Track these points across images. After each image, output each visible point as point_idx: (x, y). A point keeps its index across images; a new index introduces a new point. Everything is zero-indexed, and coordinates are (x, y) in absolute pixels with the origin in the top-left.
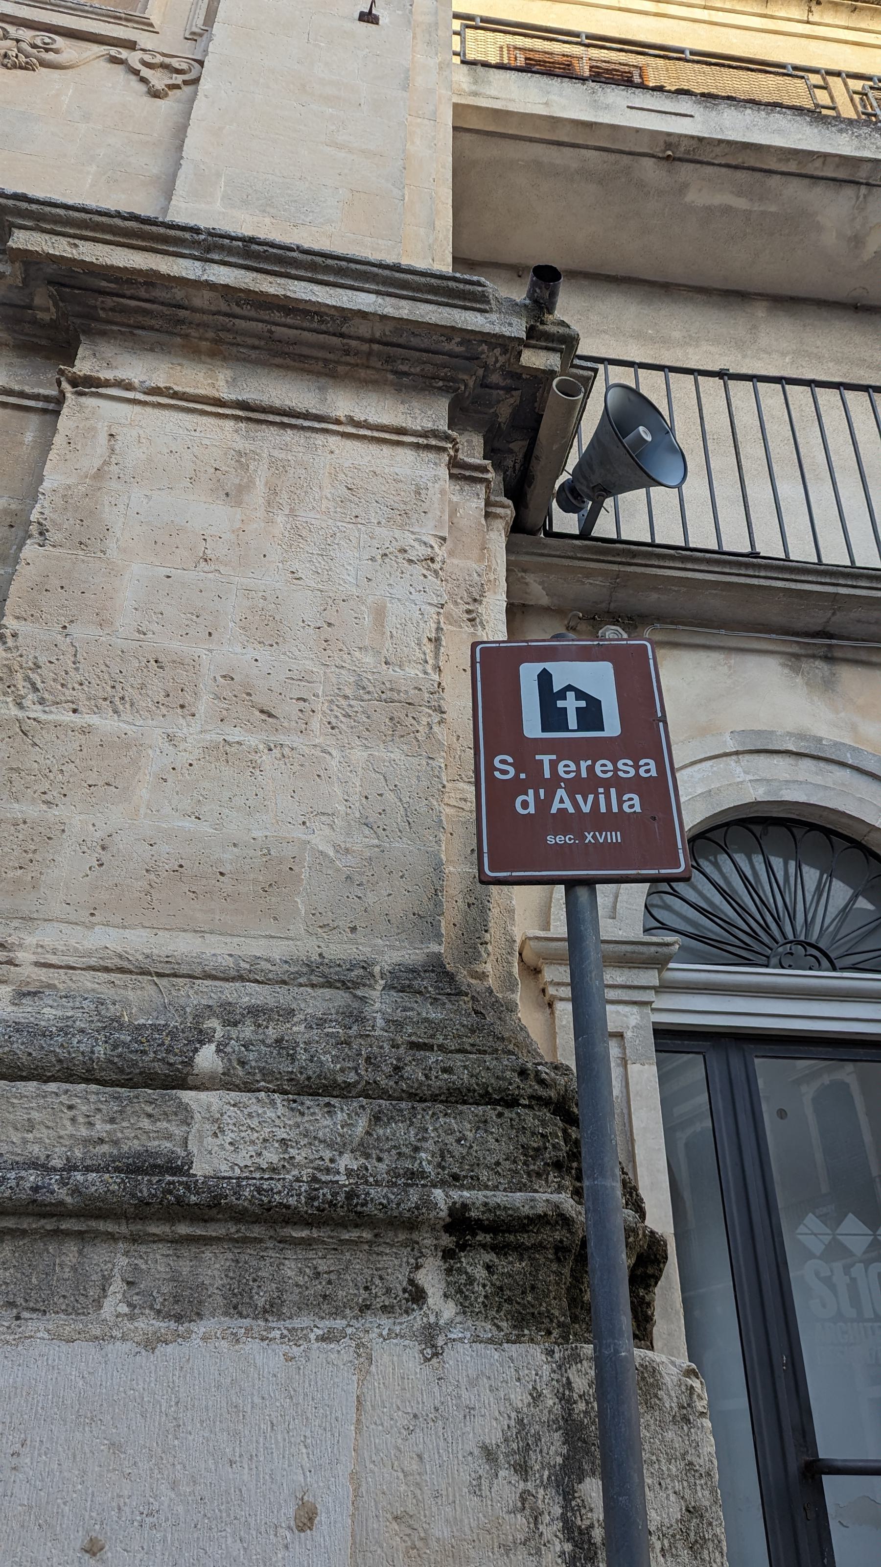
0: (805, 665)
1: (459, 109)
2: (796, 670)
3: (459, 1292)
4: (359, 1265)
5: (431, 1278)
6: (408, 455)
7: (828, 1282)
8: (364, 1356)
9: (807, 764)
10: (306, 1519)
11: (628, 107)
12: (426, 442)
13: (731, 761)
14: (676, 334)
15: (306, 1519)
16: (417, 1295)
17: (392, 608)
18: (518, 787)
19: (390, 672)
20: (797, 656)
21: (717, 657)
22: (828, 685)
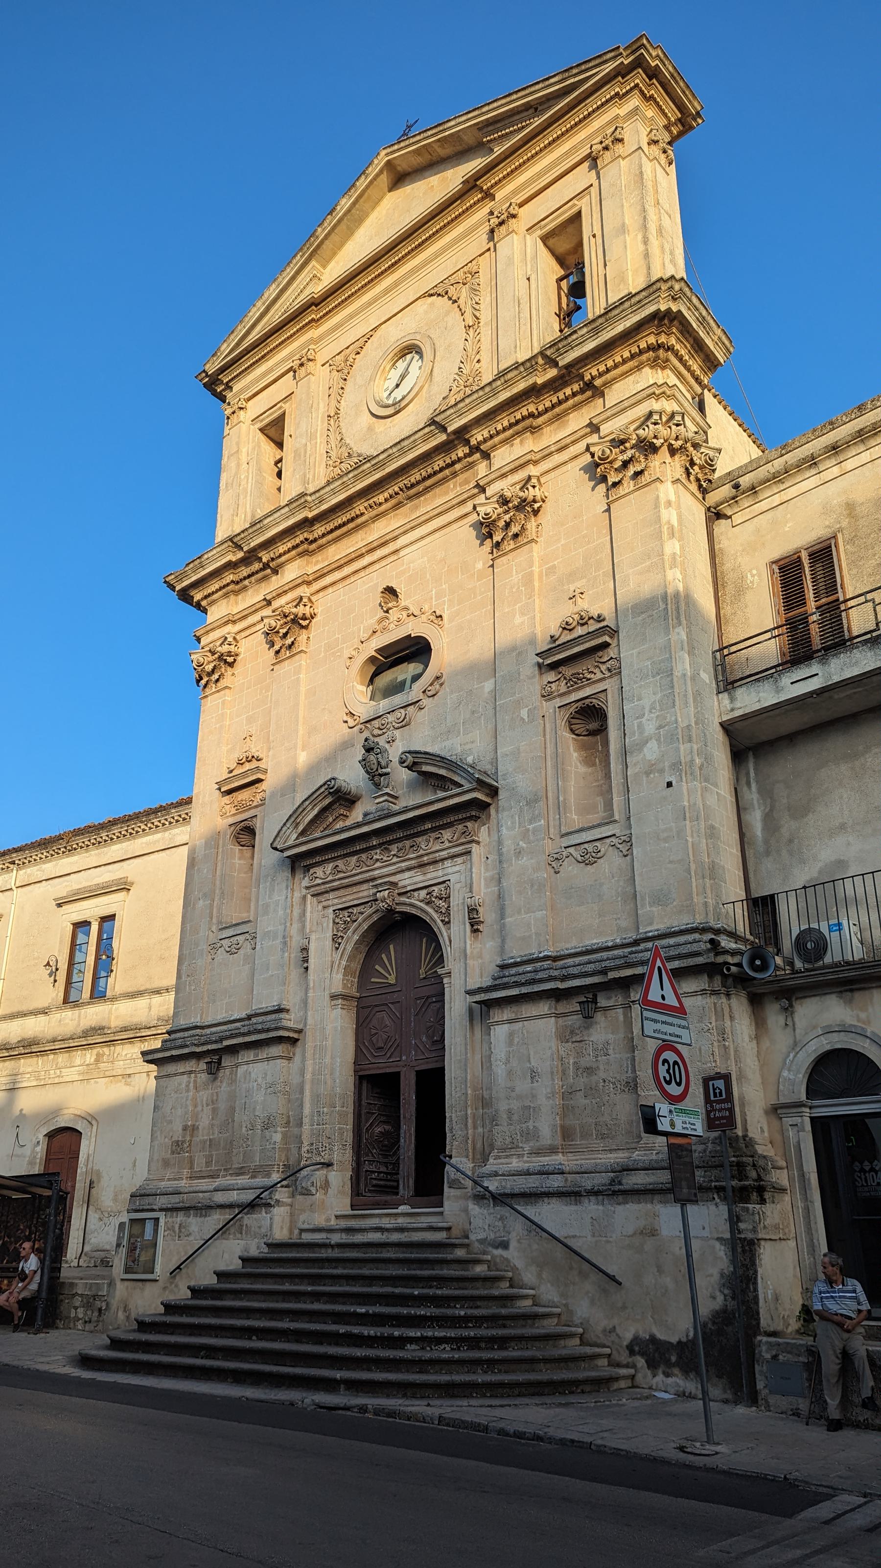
0: (844, 994)
1: (727, 727)
2: (841, 998)
3: (719, 1198)
4: (705, 1195)
5: (716, 1196)
6: (700, 997)
7: (860, 1177)
8: (708, 1208)
9: (842, 1033)
10: (704, 1228)
11: (792, 683)
12: (703, 992)
13: (822, 1037)
14: (861, 748)
15: (704, 1228)
16: (714, 1198)
17: (703, 1047)
18: (711, 1111)
19: (705, 1066)
20: (841, 992)
21: (818, 998)
22: (849, 1002)
